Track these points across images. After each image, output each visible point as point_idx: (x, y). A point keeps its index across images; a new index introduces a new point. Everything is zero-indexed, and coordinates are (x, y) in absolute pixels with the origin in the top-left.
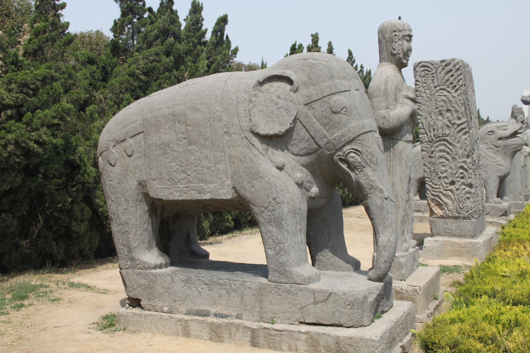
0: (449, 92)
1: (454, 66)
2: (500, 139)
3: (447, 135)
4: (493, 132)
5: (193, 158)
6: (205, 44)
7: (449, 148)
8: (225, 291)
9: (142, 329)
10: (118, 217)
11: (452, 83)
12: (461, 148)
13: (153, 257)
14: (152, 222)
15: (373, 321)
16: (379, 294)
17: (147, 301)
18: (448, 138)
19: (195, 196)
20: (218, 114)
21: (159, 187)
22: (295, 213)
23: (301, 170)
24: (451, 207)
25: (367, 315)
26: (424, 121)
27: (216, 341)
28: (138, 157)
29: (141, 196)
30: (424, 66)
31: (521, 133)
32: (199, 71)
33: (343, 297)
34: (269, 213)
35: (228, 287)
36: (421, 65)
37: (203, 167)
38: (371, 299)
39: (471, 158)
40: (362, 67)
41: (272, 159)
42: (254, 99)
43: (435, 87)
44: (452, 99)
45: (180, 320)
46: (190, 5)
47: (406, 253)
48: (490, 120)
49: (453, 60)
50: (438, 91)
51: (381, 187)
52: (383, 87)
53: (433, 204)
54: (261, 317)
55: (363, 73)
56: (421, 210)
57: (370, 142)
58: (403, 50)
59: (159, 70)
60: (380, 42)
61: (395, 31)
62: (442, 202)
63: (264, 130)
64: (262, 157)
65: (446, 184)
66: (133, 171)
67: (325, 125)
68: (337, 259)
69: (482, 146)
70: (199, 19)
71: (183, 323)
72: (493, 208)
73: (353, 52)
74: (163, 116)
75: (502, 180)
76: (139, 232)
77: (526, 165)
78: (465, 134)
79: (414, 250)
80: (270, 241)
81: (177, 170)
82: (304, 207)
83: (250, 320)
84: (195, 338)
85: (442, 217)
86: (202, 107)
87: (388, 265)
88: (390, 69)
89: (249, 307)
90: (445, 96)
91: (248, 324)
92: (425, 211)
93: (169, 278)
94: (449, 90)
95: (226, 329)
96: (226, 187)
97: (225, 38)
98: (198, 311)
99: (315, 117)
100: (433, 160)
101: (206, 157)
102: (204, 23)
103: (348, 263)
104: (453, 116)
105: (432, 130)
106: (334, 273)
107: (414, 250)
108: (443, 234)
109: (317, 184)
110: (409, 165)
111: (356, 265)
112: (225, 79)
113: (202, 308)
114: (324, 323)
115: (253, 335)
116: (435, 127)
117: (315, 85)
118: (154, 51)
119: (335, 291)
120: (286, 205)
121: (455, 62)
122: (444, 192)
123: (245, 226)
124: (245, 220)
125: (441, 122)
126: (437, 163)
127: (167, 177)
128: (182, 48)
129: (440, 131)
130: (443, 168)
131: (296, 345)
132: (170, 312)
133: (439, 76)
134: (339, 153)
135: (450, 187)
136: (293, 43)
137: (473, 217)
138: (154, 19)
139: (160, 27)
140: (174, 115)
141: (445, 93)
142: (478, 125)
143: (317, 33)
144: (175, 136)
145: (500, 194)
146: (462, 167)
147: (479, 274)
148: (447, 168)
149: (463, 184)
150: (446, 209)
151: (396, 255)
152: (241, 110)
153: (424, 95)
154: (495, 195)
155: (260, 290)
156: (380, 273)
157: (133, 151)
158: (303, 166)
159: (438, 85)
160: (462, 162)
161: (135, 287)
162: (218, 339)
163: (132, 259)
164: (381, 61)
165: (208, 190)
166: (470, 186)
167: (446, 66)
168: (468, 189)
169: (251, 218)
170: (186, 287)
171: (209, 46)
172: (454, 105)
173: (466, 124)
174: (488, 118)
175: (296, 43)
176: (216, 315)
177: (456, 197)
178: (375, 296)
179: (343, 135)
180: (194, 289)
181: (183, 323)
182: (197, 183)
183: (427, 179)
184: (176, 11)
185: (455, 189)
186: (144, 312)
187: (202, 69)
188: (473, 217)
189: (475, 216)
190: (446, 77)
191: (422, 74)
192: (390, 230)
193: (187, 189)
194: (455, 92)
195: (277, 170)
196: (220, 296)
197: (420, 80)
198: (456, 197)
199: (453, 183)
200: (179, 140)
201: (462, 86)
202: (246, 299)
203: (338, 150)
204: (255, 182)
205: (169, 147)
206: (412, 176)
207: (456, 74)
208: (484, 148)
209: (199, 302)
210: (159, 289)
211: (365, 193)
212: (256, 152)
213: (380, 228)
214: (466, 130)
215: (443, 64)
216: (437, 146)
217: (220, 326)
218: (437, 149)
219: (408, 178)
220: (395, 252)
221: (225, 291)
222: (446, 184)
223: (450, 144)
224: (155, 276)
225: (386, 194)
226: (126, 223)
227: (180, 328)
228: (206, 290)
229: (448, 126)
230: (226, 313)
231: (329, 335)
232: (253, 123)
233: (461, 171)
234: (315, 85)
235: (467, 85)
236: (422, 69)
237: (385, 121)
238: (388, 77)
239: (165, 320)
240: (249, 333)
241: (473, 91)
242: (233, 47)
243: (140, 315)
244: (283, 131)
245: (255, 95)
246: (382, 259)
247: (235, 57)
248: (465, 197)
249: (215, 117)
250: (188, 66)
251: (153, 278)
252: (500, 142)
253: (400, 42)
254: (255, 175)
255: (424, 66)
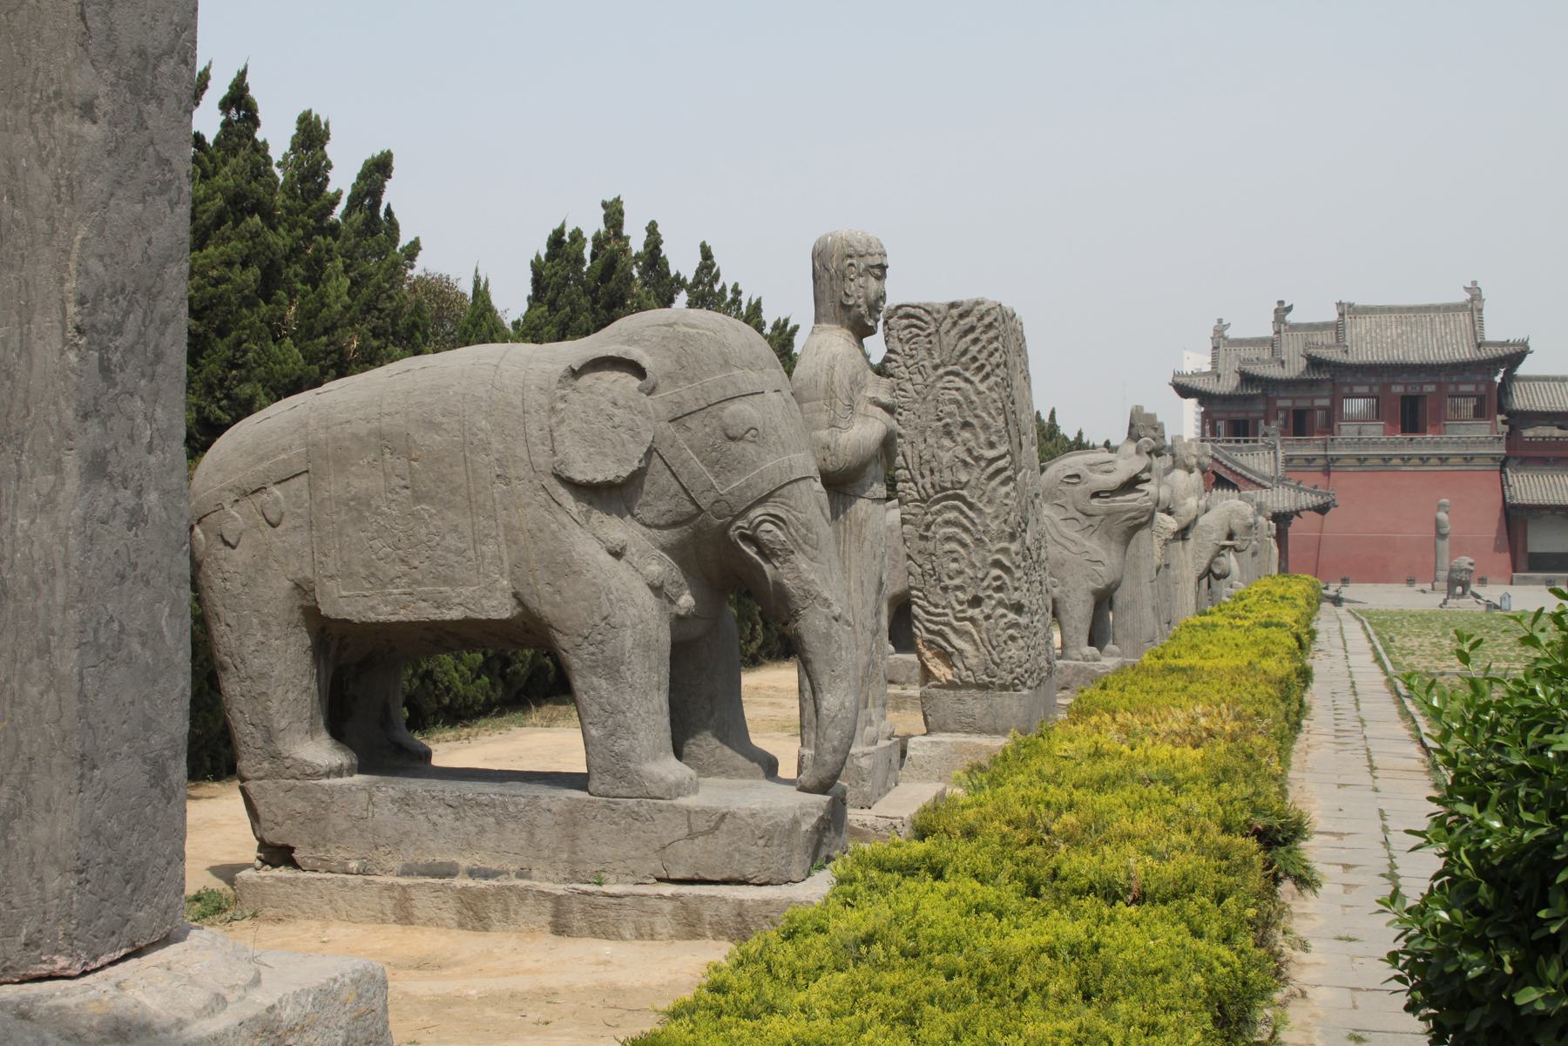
0: (967, 380)
1: (981, 319)
2: (1096, 495)
3: (964, 486)
4: (1077, 476)
5: (424, 531)
6: (334, 230)
7: (967, 517)
8: (492, 820)
9: (298, 913)
10: (243, 661)
11: (974, 359)
12: (997, 517)
13: (320, 751)
14: (318, 674)
15: (809, 875)
16: (821, 819)
17: (309, 849)
18: (964, 492)
19: (428, 613)
20: (481, 435)
21: (344, 593)
22: (647, 647)
23: (660, 557)
24: (972, 661)
25: (799, 860)
26: (907, 449)
27: (474, 929)
28: (295, 528)
29: (297, 615)
30: (908, 316)
31: (1148, 481)
32: (329, 306)
33: (750, 821)
34: (592, 649)
35: (499, 810)
36: (900, 312)
37: (448, 550)
38: (807, 825)
39: (1019, 541)
40: (737, 292)
41: (600, 533)
42: (561, 405)
43: (936, 368)
44: (974, 398)
45: (390, 887)
46: (295, 125)
47: (873, 748)
48: (1085, 440)
49: (978, 303)
50: (941, 377)
51: (826, 594)
52: (823, 379)
53: (928, 654)
54: (574, 872)
55: (739, 308)
56: (896, 678)
57: (805, 500)
58: (867, 298)
59: (229, 304)
60: (816, 278)
61: (850, 256)
62: (950, 649)
63: (584, 472)
64: (578, 530)
65: (961, 603)
66: (282, 558)
67: (711, 464)
68: (728, 751)
69: (1047, 511)
70: (319, 163)
71: (396, 894)
72: (1079, 672)
73: (714, 252)
74: (355, 436)
75: (1104, 600)
76: (291, 696)
77: (1167, 566)
78: (1004, 483)
79: (888, 743)
80: (595, 709)
81: (387, 555)
82: (665, 637)
83: (548, 879)
84: (424, 924)
85: (951, 685)
86: (444, 420)
87: (840, 757)
88: (837, 340)
89: (546, 853)
90: (958, 389)
91: (547, 887)
92: (909, 681)
93: (363, 796)
94: (967, 375)
95: (497, 901)
96: (498, 594)
97: (382, 214)
98: (429, 865)
99: (691, 447)
100: (930, 546)
101: (455, 529)
102: (331, 174)
103: (752, 760)
104: (977, 438)
105: (927, 473)
106: (723, 781)
107: (888, 743)
108: (953, 726)
109: (690, 587)
110: (878, 553)
111: (769, 766)
112: (495, 362)
113: (439, 859)
114: (709, 877)
115: (558, 910)
116: (934, 464)
117: (691, 381)
118: (222, 254)
119: (733, 808)
120: (629, 632)
121: (983, 308)
122: (956, 624)
123: (435, 724)
124: (435, 706)
125: (949, 451)
126: (939, 552)
127: (363, 572)
128: (281, 243)
129: (947, 475)
130: (954, 566)
131: (651, 924)
132: (363, 872)
133: (945, 340)
134: (739, 523)
135: (970, 612)
136: (557, 226)
137: (1024, 684)
138: (210, 167)
139: (226, 188)
140: (381, 436)
141: (960, 383)
142: (1037, 461)
143: (618, 200)
144: (382, 483)
145: (1097, 636)
146: (997, 564)
147: (1018, 753)
148: (963, 565)
149: (1000, 603)
150: (960, 665)
151: (852, 751)
152: (533, 429)
153: (909, 386)
154: (1084, 639)
155: (571, 813)
156: (823, 773)
157: (282, 514)
158: (664, 549)
159: (943, 364)
160: (998, 551)
161: (280, 819)
162: (477, 924)
163: (275, 757)
164: (817, 320)
165: (457, 600)
166: (1018, 608)
167: (961, 316)
168: (1011, 616)
169: (451, 700)
170: (401, 815)
171: (347, 239)
172: (978, 412)
173: (1008, 458)
174: (1080, 434)
175: (563, 226)
176: (472, 873)
177: (984, 636)
178: (814, 820)
179: (748, 486)
180: (422, 817)
181: (396, 894)
182: (434, 584)
183: (914, 592)
184: (265, 143)
185: (981, 617)
186: (301, 875)
187: (336, 302)
188: (1024, 684)
189: (1029, 683)
190: (962, 345)
191: (905, 334)
192: (845, 684)
193: (410, 598)
194: (982, 381)
195: (610, 558)
196: (482, 831)
197: (899, 350)
198: (984, 636)
199: (976, 602)
200: (392, 491)
201: (998, 366)
202: (539, 834)
203: (737, 517)
204: (563, 583)
205: (369, 505)
206: (884, 577)
207: (984, 337)
208: (1057, 518)
209: (432, 845)
210: (339, 821)
211: (793, 607)
212: (566, 519)
213: (824, 680)
214: (1008, 473)
215: (955, 312)
216: (939, 513)
217: (483, 894)
218: (939, 519)
219: (876, 580)
220: (852, 738)
221: (492, 820)
222: (961, 603)
223: (971, 506)
224: (330, 792)
225: (837, 610)
226: (262, 675)
227: (389, 905)
228: (449, 819)
229: (965, 463)
230: (494, 866)
231: (723, 900)
232: (560, 456)
233: (996, 572)
234: (691, 381)
235: (1010, 364)
236: (905, 322)
237: (827, 454)
238: (834, 358)
239: (353, 888)
240: (549, 904)
241: (1027, 378)
242: (404, 240)
243: (292, 882)
244: (625, 475)
245: (563, 399)
246: (827, 745)
247: (412, 267)
248: (1005, 637)
249: (476, 442)
250: (297, 291)
251: (326, 798)
252: (1095, 502)
253: (861, 280)
254: (563, 566)
255: (908, 316)
